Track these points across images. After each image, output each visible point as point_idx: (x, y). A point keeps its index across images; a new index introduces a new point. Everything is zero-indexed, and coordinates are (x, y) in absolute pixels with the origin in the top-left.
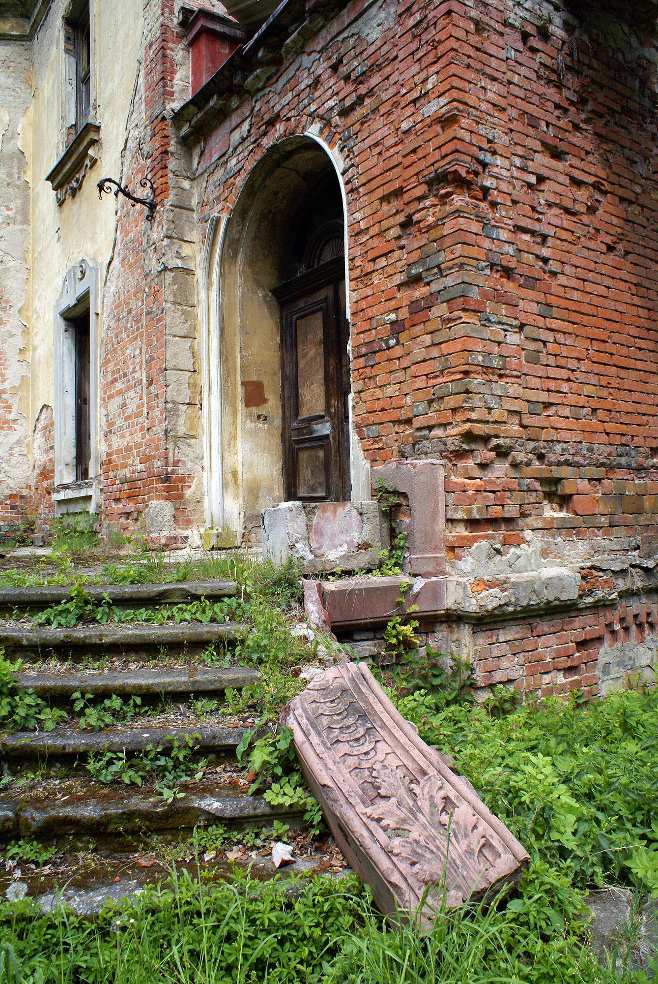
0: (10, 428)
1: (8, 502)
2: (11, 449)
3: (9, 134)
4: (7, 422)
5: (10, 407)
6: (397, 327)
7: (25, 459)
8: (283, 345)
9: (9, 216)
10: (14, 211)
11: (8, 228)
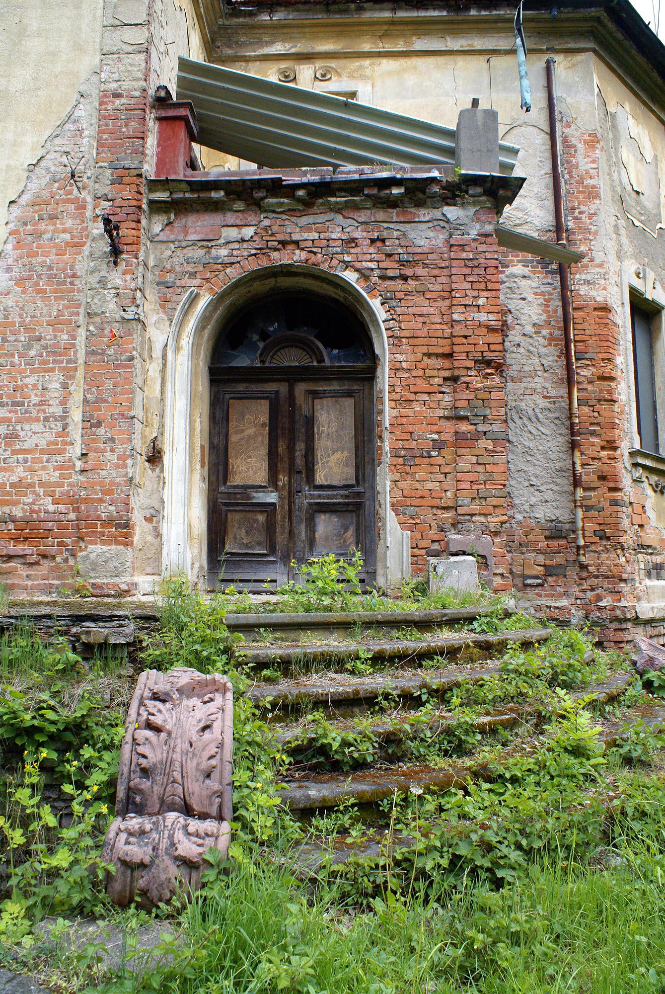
6: (439, 445)
8: (213, 418)
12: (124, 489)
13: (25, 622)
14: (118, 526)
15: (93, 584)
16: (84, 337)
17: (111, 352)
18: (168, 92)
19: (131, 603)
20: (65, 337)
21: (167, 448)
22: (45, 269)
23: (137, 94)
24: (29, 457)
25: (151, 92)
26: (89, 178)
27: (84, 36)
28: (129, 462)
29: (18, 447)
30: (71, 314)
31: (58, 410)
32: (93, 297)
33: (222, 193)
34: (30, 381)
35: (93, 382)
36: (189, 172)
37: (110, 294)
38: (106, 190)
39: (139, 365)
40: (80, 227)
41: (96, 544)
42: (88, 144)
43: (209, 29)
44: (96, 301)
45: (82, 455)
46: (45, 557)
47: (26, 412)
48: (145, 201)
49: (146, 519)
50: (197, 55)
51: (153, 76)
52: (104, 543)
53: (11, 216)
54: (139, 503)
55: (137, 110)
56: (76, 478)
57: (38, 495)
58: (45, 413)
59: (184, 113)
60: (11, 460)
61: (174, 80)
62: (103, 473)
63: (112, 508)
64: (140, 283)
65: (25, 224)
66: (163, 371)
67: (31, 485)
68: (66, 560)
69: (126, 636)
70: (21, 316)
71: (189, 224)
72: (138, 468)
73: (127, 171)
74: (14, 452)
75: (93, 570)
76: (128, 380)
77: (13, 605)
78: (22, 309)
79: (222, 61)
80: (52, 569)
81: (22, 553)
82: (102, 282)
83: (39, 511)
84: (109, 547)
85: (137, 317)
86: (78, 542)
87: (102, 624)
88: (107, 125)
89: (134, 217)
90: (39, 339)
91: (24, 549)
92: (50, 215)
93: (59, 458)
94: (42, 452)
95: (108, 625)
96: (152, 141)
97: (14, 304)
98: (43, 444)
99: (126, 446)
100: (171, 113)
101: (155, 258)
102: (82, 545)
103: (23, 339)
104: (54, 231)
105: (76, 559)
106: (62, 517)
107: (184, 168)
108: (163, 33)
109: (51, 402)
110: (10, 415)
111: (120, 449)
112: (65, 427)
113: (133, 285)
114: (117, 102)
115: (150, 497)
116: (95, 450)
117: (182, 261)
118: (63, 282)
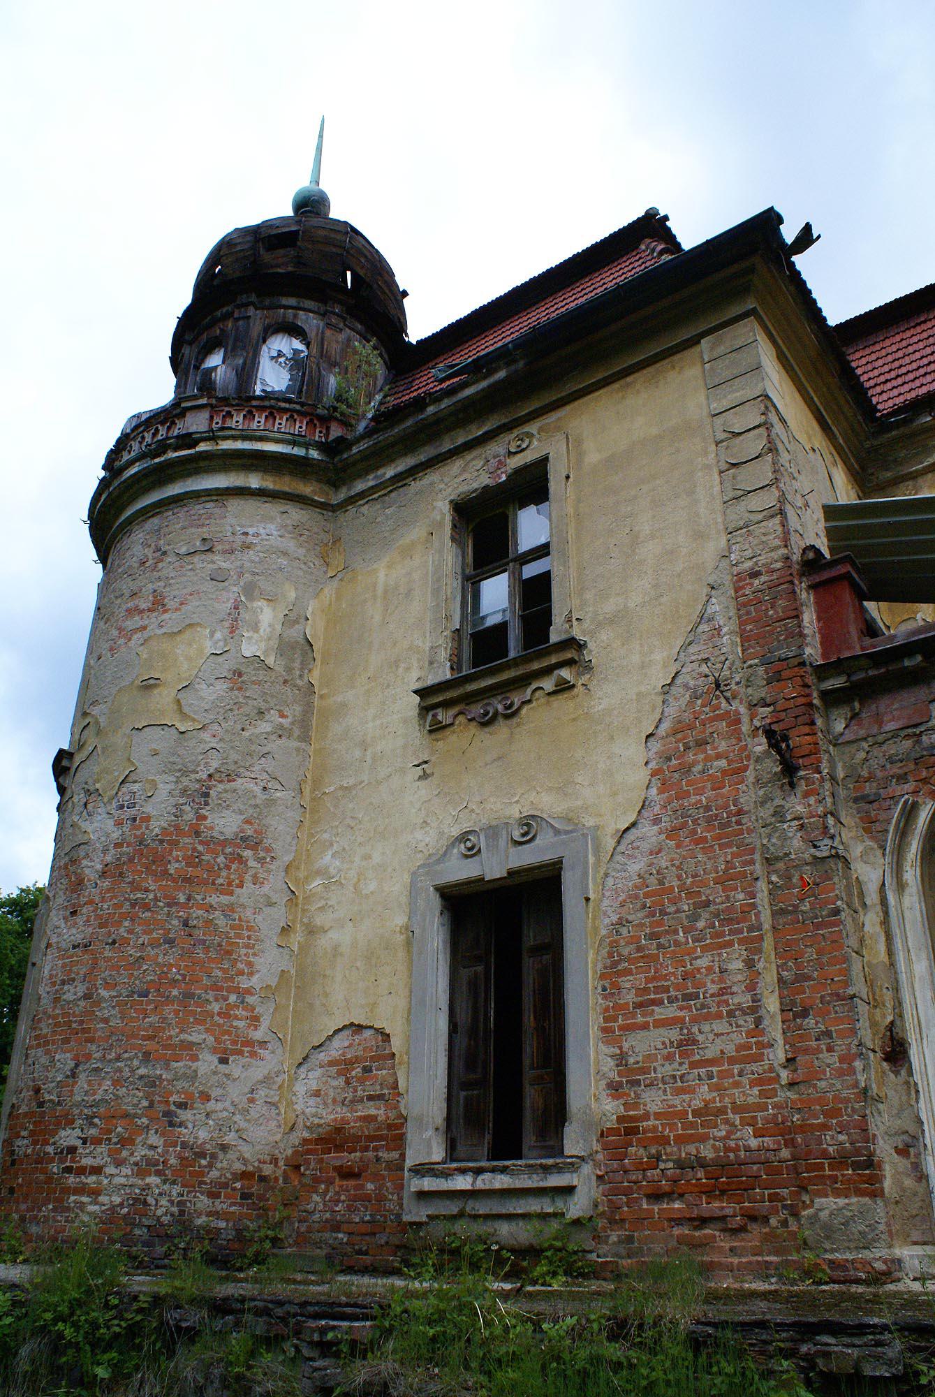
0: (253, 1055)
1: (238, 1185)
2: (252, 1091)
3: (292, 616)
4: (249, 1043)
5: (256, 1019)
7: (274, 1111)
9: (281, 726)
10: (289, 720)
11: (279, 742)
12: (857, 1106)
13: (729, 1334)
14: (856, 1166)
15: (831, 1262)
16: (766, 893)
17: (806, 907)
18: (818, 552)
19: (896, 1294)
20: (741, 896)
21: (912, 1037)
22: (701, 810)
23: (778, 565)
24: (714, 1069)
25: (796, 557)
26: (738, 683)
27: (703, 521)
28: (858, 1064)
29: (697, 1057)
30: (745, 864)
31: (744, 999)
32: (769, 836)
33: (919, 658)
34: (703, 962)
35: (786, 952)
36: (868, 641)
37: (790, 828)
38: (763, 693)
39: (849, 920)
40: (737, 747)
41: (826, 1196)
42: (729, 642)
43: (854, 456)
44: (774, 840)
45: (788, 1060)
46: (753, 1218)
47: (703, 1006)
48: (815, 694)
49: (899, 1151)
50: (845, 494)
51: (794, 538)
52: (837, 1193)
53: (650, 753)
54: (883, 1124)
55: (784, 584)
56: (783, 1095)
57: (733, 1125)
58: (728, 1005)
59: (843, 571)
60: (691, 1077)
61: (823, 534)
62: (822, 1084)
63: (842, 1138)
64: (829, 805)
65: (669, 759)
66: (886, 922)
67: (722, 1111)
68: (785, 1223)
69: (890, 1363)
70: (679, 878)
71: (882, 709)
72: (870, 1073)
73: (785, 663)
74: (694, 1065)
75: (828, 1237)
76: (836, 943)
77: (713, 1297)
78: (679, 868)
79: (882, 488)
80: (771, 1237)
81: (720, 1214)
82: (779, 814)
83: (737, 1148)
84: (847, 1201)
85: (833, 852)
86: (799, 1193)
87: (847, 1340)
88: (748, 613)
89: (805, 719)
90: (707, 904)
91: (723, 1208)
92: (696, 741)
93: (754, 1067)
94: (732, 1061)
95: (857, 1341)
96: (809, 617)
97: (669, 864)
98: (730, 1050)
99: (848, 1041)
100: (826, 575)
101: (844, 767)
102: (806, 1198)
103: (686, 908)
104: (705, 760)
105: (798, 1220)
106: (771, 1155)
107: (859, 639)
108: (796, 485)
109: (734, 989)
110: (682, 1014)
111: (840, 1046)
112: (758, 1021)
113: (820, 810)
114: (756, 582)
115: (898, 1115)
116: (806, 1051)
117: (882, 761)
118: (726, 824)
